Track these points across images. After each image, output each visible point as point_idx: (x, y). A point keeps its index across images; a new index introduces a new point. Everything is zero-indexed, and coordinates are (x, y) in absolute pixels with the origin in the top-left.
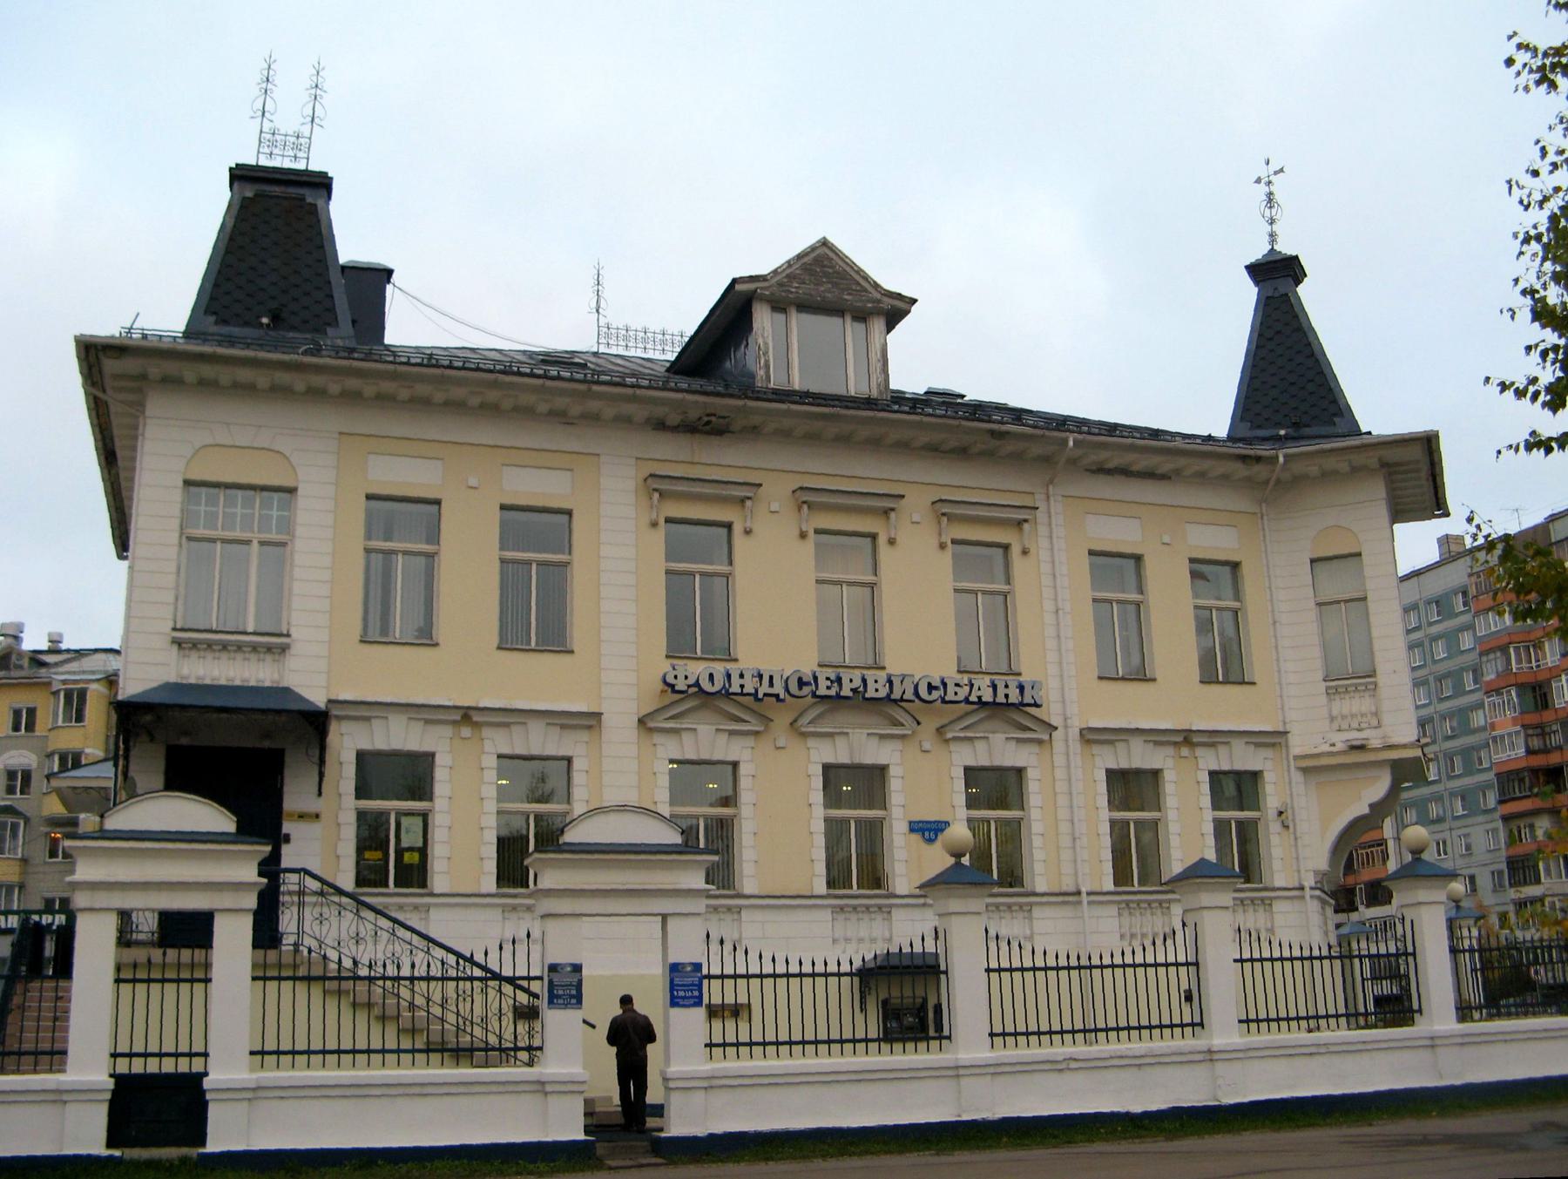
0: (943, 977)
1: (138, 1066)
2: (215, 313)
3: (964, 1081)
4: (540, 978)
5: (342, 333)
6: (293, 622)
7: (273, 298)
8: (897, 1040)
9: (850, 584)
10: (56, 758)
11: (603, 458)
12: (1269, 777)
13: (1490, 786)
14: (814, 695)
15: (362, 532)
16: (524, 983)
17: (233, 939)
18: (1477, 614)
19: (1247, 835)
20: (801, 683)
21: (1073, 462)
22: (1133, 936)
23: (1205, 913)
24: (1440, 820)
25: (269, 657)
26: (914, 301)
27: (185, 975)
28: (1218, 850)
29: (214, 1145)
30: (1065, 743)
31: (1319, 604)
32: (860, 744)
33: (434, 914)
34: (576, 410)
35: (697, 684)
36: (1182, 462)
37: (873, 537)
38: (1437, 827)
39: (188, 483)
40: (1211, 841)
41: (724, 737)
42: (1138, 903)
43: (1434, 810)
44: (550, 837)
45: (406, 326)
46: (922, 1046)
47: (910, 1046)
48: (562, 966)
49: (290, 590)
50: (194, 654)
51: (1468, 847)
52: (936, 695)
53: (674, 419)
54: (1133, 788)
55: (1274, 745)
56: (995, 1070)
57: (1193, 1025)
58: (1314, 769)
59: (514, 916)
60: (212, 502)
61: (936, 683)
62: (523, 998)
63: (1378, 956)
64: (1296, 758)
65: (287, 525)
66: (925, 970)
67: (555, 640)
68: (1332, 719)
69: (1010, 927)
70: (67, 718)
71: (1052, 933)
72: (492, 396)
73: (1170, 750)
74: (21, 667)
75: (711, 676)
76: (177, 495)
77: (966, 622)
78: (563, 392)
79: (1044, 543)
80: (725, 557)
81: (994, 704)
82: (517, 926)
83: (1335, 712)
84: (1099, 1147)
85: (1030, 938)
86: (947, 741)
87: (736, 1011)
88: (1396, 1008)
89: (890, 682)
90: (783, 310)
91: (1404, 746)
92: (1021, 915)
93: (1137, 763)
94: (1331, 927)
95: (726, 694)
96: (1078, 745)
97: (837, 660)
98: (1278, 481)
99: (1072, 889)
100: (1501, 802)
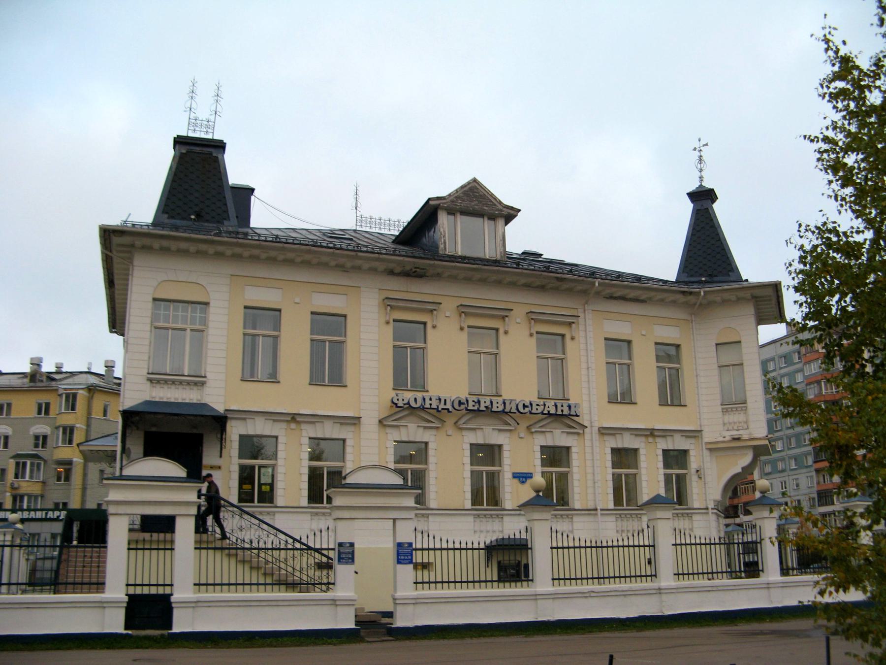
0: (530, 551)
1: (138, 591)
2: (167, 213)
3: (539, 601)
4: (333, 549)
5: (231, 225)
6: (208, 369)
7: (197, 205)
8: (507, 581)
9: (485, 353)
10: (61, 429)
11: (363, 289)
12: (692, 453)
13: (810, 454)
14: (467, 409)
15: (242, 324)
16: (325, 552)
17: (185, 529)
18: (805, 363)
19: (681, 480)
20: (460, 403)
21: (598, 293)
22: (622, 531)
23: (659, 521)
24: (783, 471)
25: (195, 388)
26: (520, 210)
27: (162, 546)
28: (666, 491)
29: (177, 629)
30: (591, 434)
31: (719, 367)
32: (489, 434)
33: (277, 516)
34: (349, 264)
35: (408, 403)
36: (652, 294)
37: (497, 330)
38: (782, 474)
39: (155, 300)
40: (662, 484)
41: (421, 430)
42: (626, 515)
43: (780, 466)
44: (337, 477)
45: (261, 217)
46: (519, 584)
47: (513, 584)
48: (345, 543)
49: (206, 354)
50: (158, 386)
51: (797, 485)
52: (527, 410)
53: (398, 270)
54: (624, 458)
55: (695, 437)
56: (554, 596)
57: (651, 576)
58: (714, 449)
59: (316, 518)
60: (167, 309)
61: (527, 404)
62: (324, 559)
63: (748, 543)
64: (706, 443)
65: (204, 321)
66: (521, 547)
67: (337, 380)
68: (724, 424)
69: (562, 526)
70: (67, 408)
71: (582, 530)
72: (307, 257)
73: (643, 439)
74: (42, 381)
75: (415, 399)
76: (150, 305)
77: (542, 373)
78: (343, 256)
79: (582, 334)
80: (423, 339)
81: (556, 415)
82: (322, 523)
83: (726, 421)
84: (606, 634)
85: (572, 532)
86: (532, 433)
87: (425, 566)
88: (753, 569)
89: (504, 403)
90: (453, 214)
91: (760, 439)
92: (567, 520)
93: (626, 445)
94: (723, 528)
95: (423, 408)
97: (477, 391)
98: (701, 304)
99: (592, 507)
100: (815, 462)
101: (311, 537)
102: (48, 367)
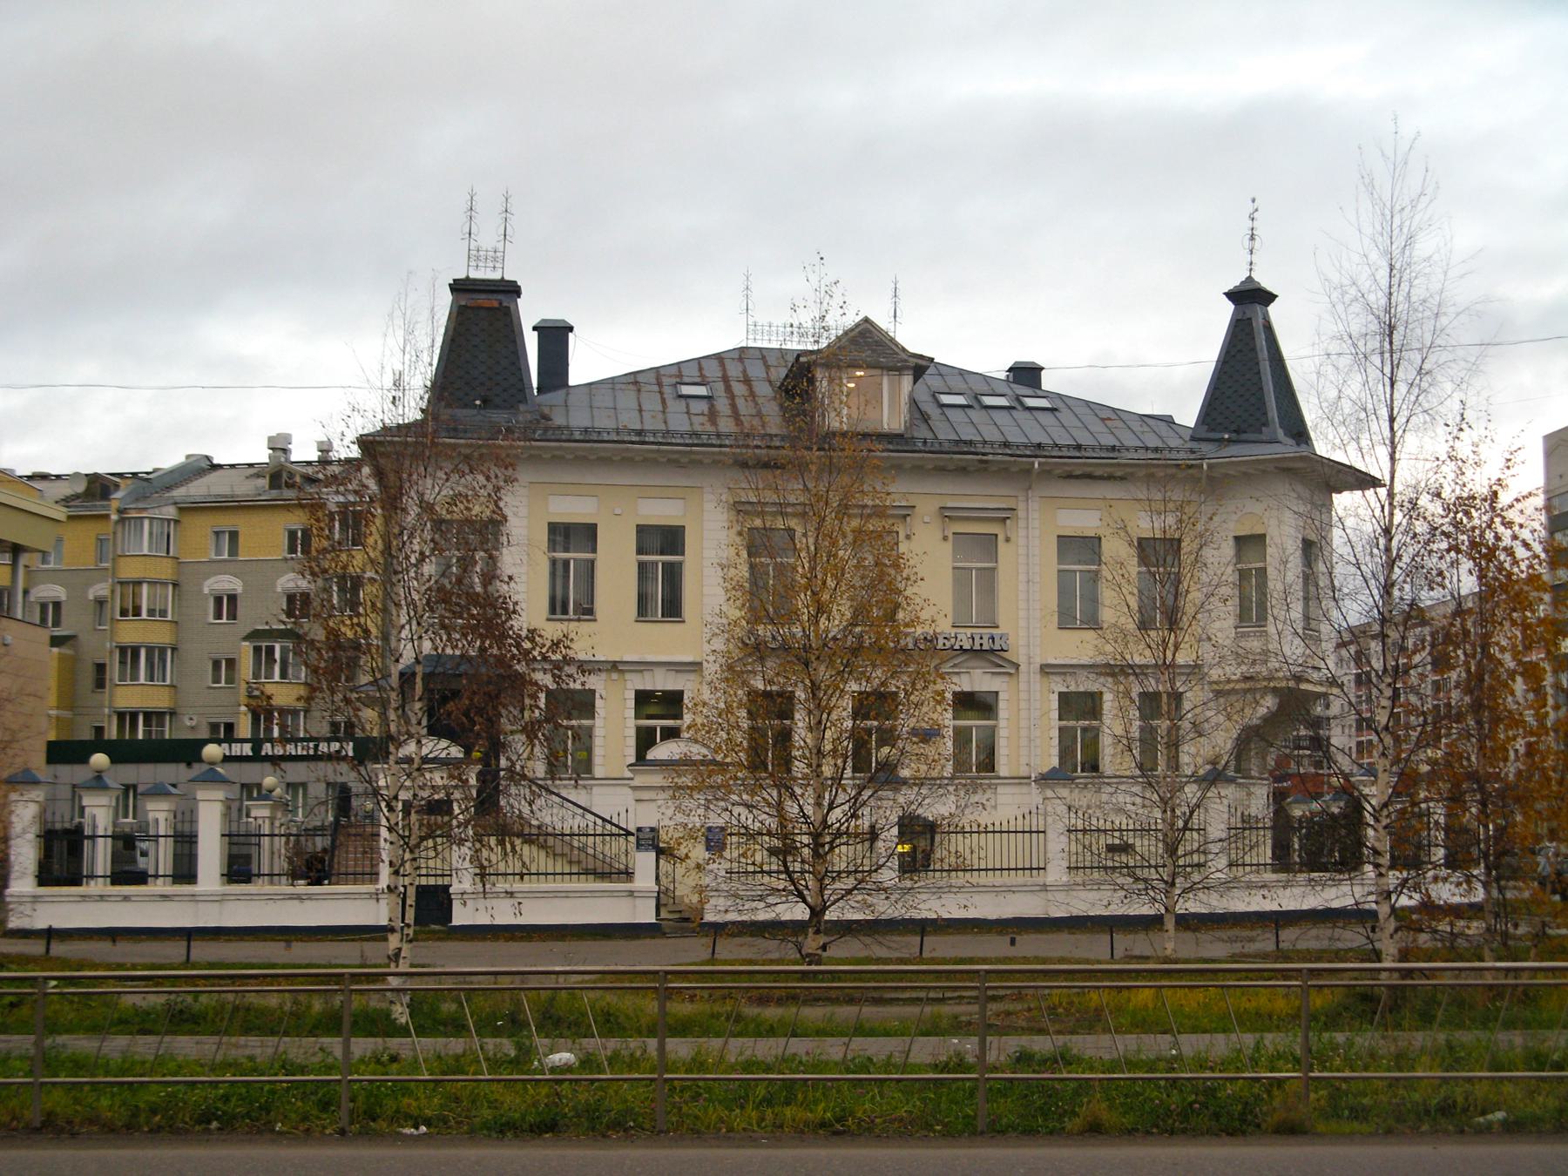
29: (456, 922)
30: (1029, 676)
34: (684, 460)
79: (1022, 533)
96: (1038, 676)
101: (623, 815)
102: (303, 451)
